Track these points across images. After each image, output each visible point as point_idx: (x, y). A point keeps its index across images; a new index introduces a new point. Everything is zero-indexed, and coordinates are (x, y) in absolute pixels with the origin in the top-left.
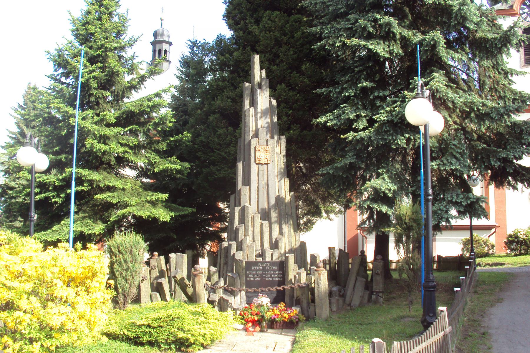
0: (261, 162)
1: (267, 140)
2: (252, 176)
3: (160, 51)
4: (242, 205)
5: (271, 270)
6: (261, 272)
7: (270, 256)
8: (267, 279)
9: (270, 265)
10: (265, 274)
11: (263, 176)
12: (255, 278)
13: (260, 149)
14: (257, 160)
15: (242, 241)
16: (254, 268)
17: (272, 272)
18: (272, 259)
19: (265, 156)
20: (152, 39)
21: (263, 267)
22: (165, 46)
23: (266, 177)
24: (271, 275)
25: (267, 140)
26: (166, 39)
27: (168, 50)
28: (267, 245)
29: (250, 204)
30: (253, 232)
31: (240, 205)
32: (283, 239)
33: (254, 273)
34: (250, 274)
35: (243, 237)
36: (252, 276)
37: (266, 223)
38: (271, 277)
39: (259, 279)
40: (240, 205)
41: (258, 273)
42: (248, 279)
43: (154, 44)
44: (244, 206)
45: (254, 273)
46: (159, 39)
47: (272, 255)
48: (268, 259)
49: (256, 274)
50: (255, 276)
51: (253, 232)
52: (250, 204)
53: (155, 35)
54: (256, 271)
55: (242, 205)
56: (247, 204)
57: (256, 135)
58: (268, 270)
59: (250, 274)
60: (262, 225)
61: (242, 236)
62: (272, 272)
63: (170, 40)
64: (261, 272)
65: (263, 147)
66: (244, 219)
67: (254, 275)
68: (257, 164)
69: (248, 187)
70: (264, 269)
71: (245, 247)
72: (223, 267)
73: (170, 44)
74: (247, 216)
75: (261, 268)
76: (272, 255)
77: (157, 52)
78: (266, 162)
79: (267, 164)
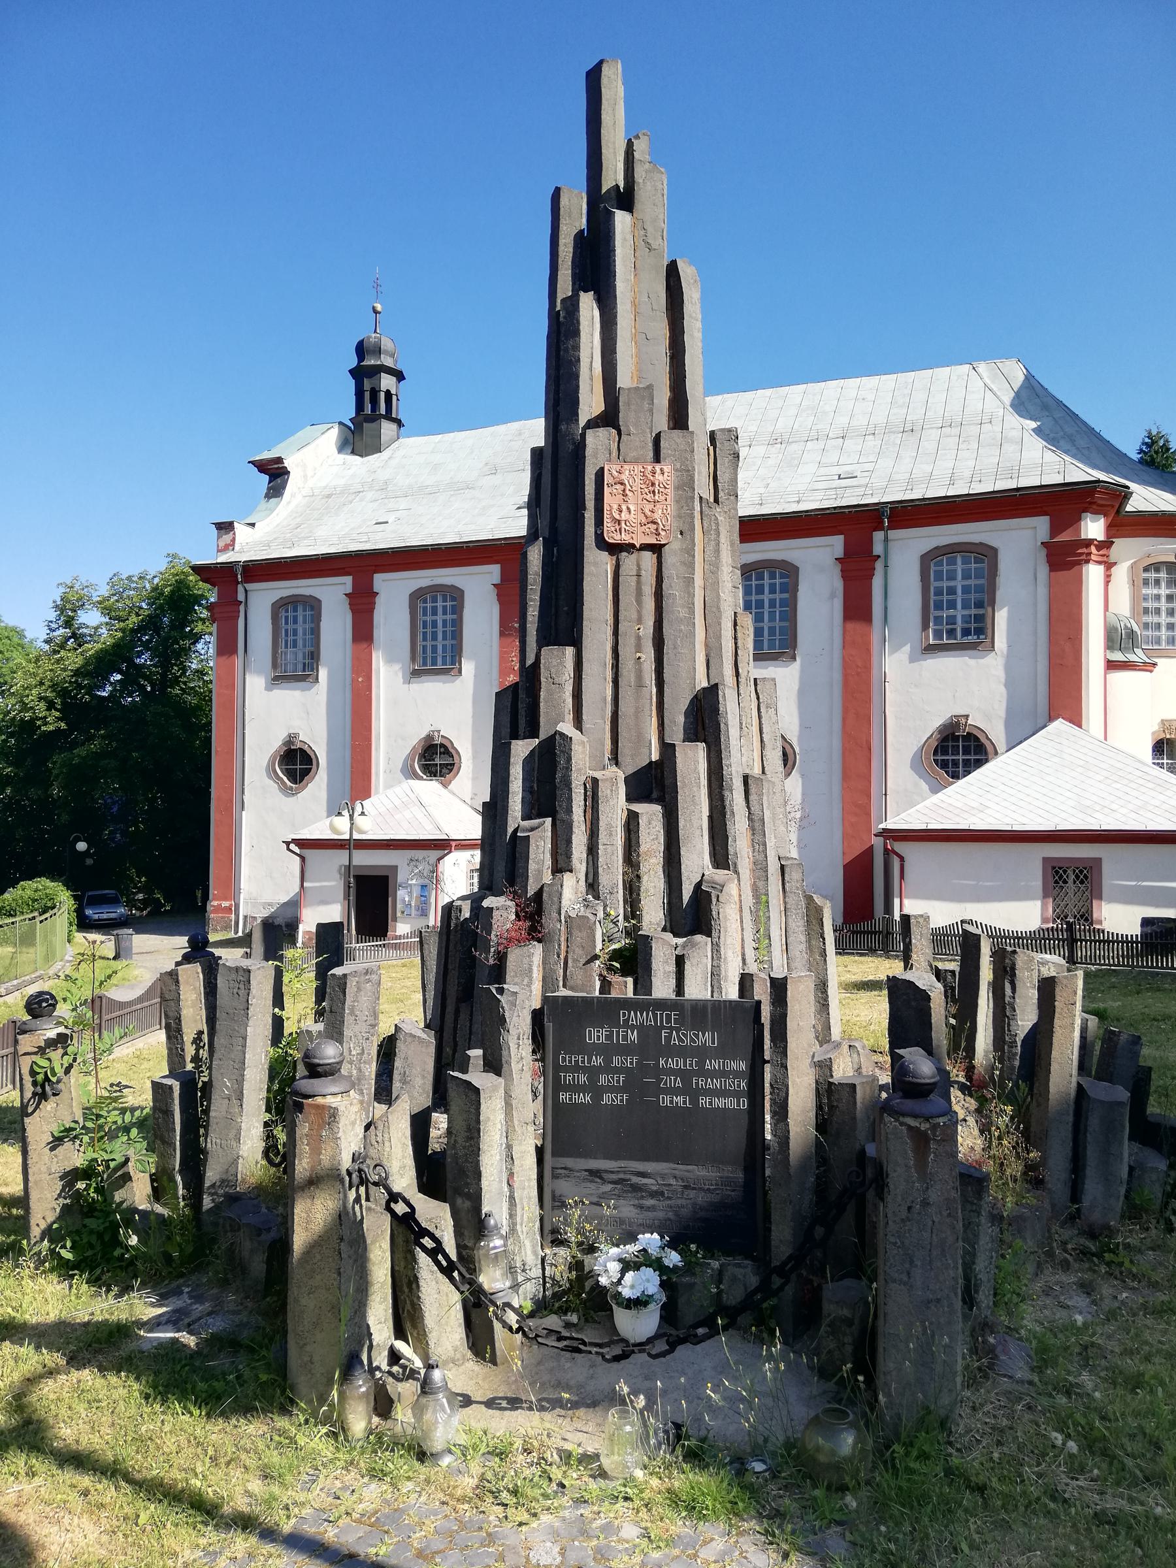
0: (625, 538)
1: (657, 441)
2: (587, 598)
3: (375, 393)
4: (544, 733)
5: (682, 1052)
6: (631, 1061)
7: (672, 968)
8: (665, 1101)
9: (681, 1021)
10: (658, 1072)
11: (639, 601)
12: (597, 1091)
13: (625, 477)
14: (608, 523)
15: (539, 894)
16: (596, 1035)
17: (691, 1063)
18: (680, 988)
19: (648, 508)
20: (353, 362)
21: (641, 1028)
22: (387, 382)
23: (649, 604)
24: (685, 1075)
25: (657, 441)
26: (387, 361)
27: (393, 392)
28: (653, 914)
29: (578, 723)
30: (592, 850)
31: (533, 732)
32: (732, 889)
33: (597, 1061)
34: (577, 1068)
35: (547, 878)
36: (583, 1079)
37: (651, 814)
38: (687, 1090)
39: (621, 1099)
40: (533, 732)
41: (616, 1061)
42: (564, 1097)
43: (359, 374)
44: (551, 739)
45: (597, 1061)
46: (370, 361)
47: (680, 961)
48: (662, 987)
49: (608, 1069)
50: (603, 1080)
51: (592, 850)
52: (578, 723)
53: (361, 350)
54: (607, 1050)
55: (544, 733)
56: (566, 727)
57: (609, 418)
58: (671, 1051)
59: (577, 1068)
60: (632, 820)
61: (540, 872)
62: (691, 1063)
63: (399, 367)
64: (631, 1061)
65: (638, 468)
66: (553, 797)
67: (593, 1072)
68: (615, 549)
69: (570, 651)
70: (650, 1039)
71: (550, 922)
72: (457, 1012)
73: (400, 376)
74: (568, 784)
75: (634, 1036)
76: (680, 961)
77: (367, 395)
78: (652, 540)
79: (656, 549)
